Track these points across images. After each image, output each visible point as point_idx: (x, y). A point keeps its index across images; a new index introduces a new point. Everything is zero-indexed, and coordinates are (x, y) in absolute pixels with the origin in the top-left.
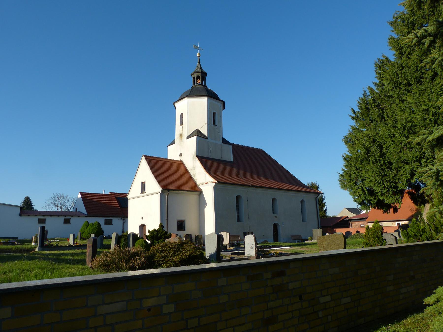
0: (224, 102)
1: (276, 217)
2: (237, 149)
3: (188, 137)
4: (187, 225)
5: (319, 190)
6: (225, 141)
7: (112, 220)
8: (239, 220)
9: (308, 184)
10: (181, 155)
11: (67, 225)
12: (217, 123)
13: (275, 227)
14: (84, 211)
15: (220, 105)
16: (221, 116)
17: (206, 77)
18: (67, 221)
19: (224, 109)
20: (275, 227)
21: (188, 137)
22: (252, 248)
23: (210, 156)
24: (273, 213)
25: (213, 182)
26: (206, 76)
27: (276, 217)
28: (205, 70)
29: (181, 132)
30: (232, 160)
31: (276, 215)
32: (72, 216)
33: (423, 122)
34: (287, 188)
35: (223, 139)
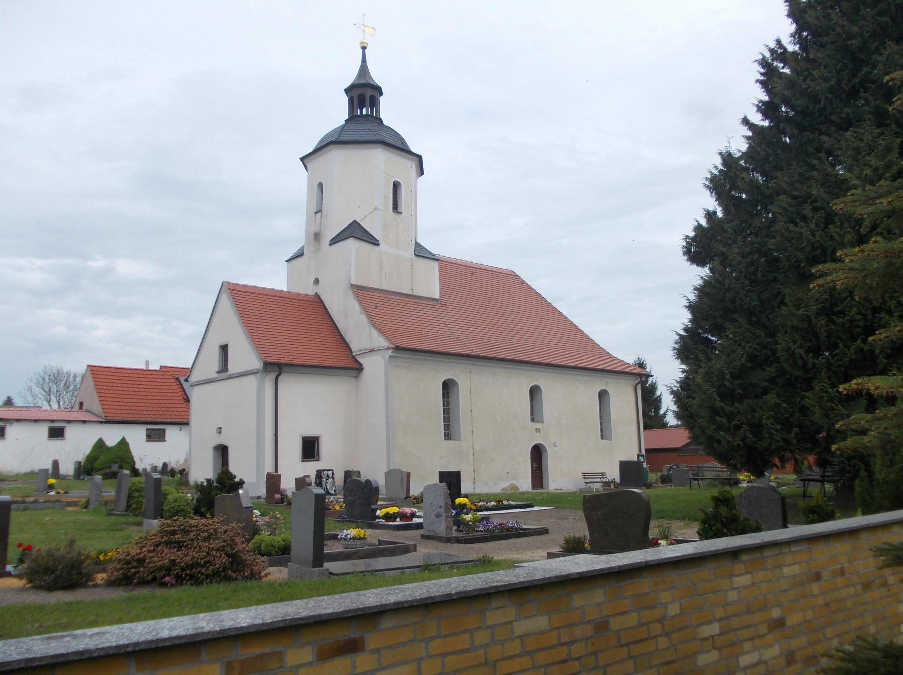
0: (420, 158)
1: (538, 430)
2: (451, 270)
3: (334, 241)
4: (325, 448)
5: (648, 370)
6: (421, 252)
7: (164, 430)
8: (448, 437)
9: (683, 372)
10: (317, 281)
11: (57, 443)
12: (403, 207)
13: (538, 453)
14: (97, 408)
15: (412, 166)
16: (414, 192)
17: (382, 99)
18: (56, 433)
19: (422, 173)
20: (538, 453)
21: (334, 241)
22: (439, 515)
23: (384, 287)
24: (533, 420)
25: (388, 348)
26: (381, 94)
27: (538, 430)
28: (377, 76)
29: (317, 230)
30: (438, 297)
31: (538, 426)
32: (69, 422)
33: (766, 384)
34: (563, 363)
35: (418, 245)
